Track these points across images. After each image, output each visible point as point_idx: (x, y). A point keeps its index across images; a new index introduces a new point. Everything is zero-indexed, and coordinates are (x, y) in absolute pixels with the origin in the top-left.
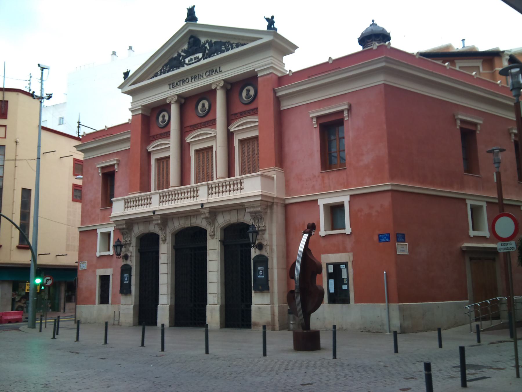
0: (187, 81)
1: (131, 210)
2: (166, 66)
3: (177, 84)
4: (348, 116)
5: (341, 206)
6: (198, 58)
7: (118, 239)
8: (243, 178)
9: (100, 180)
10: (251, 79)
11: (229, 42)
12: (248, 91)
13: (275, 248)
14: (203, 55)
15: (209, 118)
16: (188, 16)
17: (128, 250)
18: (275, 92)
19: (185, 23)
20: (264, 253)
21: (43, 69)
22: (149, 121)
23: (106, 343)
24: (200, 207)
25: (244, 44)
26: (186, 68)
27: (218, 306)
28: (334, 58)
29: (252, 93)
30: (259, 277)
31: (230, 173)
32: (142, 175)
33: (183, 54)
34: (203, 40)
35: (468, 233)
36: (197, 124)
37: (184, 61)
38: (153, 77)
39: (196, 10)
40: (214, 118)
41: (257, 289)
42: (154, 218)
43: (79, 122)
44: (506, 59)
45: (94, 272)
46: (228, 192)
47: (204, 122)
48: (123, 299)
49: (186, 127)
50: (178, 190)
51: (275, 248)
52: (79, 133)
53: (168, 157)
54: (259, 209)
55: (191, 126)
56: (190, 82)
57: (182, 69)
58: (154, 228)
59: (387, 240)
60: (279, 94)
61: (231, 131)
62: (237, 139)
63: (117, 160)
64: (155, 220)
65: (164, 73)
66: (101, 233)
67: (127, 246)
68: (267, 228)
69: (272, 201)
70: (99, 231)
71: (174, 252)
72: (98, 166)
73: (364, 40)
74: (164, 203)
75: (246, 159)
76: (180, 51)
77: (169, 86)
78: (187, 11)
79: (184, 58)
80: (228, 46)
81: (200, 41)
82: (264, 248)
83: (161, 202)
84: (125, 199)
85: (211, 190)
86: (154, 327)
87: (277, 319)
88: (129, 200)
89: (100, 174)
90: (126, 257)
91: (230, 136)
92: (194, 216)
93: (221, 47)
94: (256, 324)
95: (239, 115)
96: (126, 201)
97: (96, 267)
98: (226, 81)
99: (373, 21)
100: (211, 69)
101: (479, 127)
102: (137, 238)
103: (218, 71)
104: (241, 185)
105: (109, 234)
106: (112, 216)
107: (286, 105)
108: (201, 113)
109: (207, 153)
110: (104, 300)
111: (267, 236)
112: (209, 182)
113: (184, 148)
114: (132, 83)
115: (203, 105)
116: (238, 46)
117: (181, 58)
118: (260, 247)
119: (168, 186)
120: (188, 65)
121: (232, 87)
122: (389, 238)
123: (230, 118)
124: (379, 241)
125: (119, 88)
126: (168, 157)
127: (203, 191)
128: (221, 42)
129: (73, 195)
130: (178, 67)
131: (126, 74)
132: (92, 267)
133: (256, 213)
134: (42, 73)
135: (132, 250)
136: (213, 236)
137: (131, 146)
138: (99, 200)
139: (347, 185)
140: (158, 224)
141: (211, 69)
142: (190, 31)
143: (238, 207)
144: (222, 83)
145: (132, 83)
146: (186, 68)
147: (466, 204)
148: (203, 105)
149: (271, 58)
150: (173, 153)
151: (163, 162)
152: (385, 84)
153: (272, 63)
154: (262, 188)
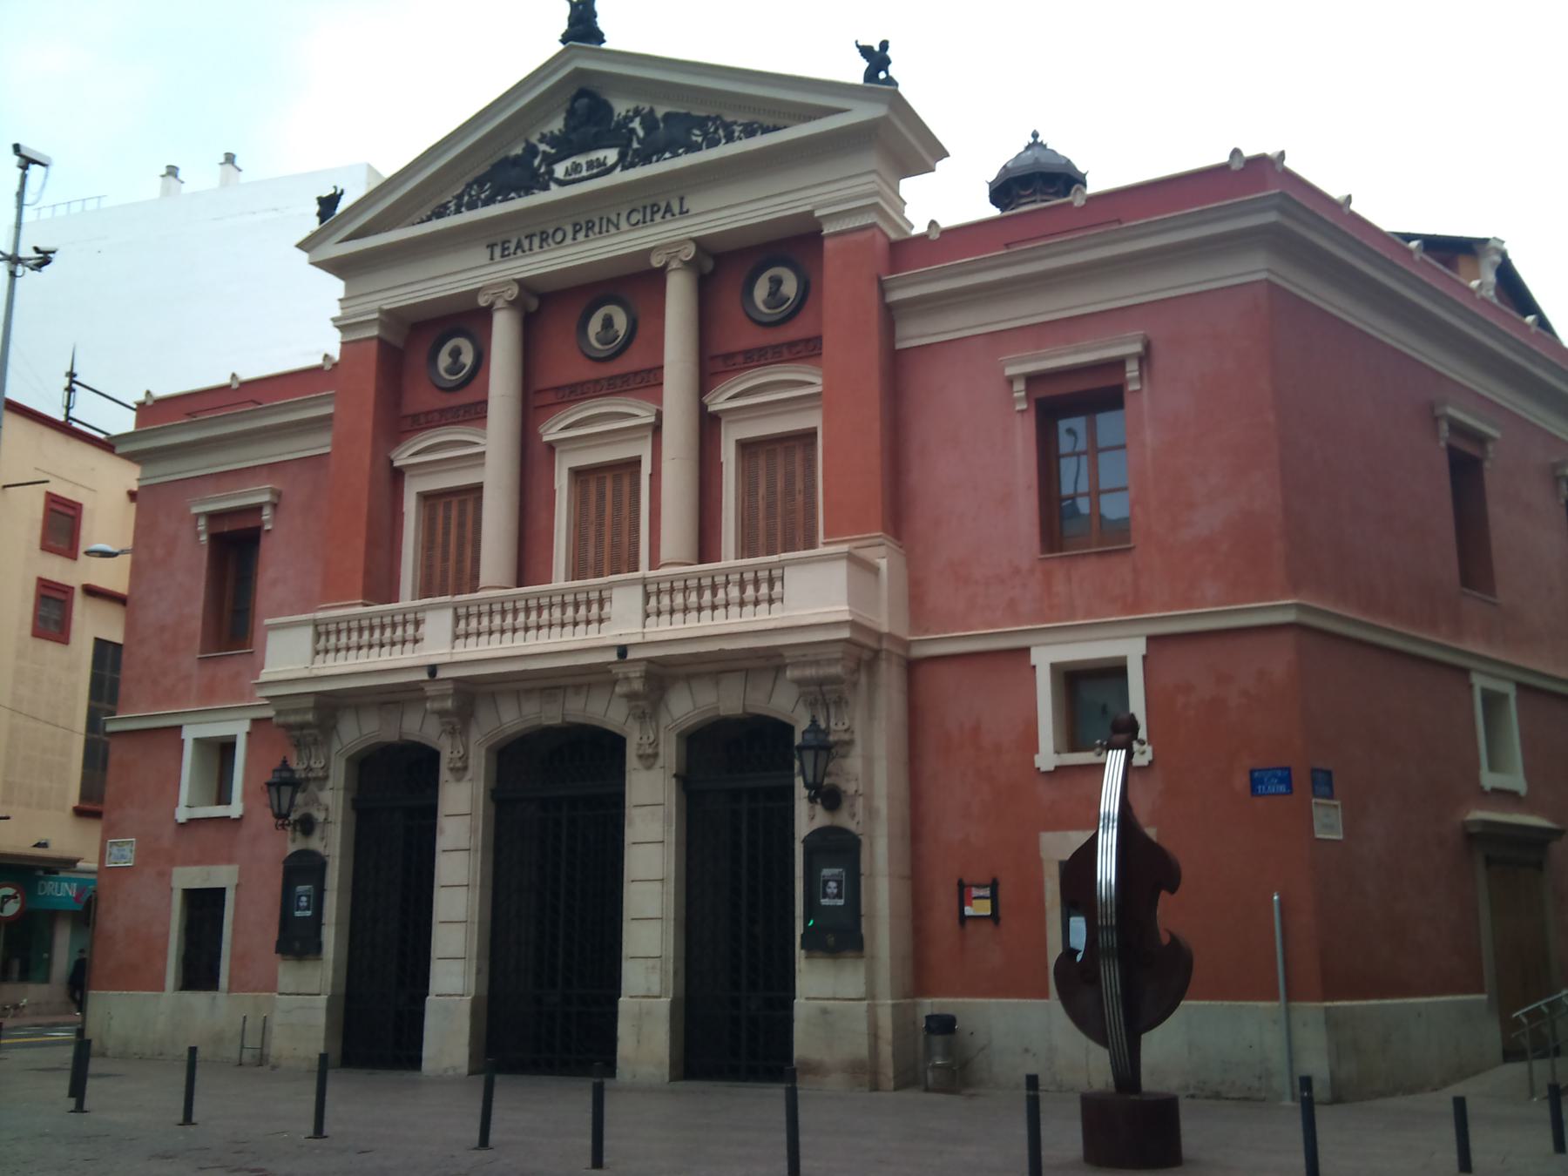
0: (559, 236)
1: (341, 662)
3: (519, 246)
4: (1141, 377)
5: (1115, 671)
7: (285, 762)
8: (782, 565)
9: (204, 555)
10: (798, 243)
11: (718, 117)
12: (777, 282)
13: (882, 804)
14: (622, 156)
15: (632, 362)
16: (570, 25)
17: (316, 801)
18: (883, 291)
19: (561, 47)
20: (843, 820)
21: (27, 162)
22: (407, 364)
23: (319, 1131)
24: (425, 677)
25: (776, 129)
26: (555, 193)
27: (665, 1001)
28: (945, 223)
29: (467, 358)
30: (825, 902)
31: (706, 548)
32: (371, 543)
33: (543, 147)
34: (621, 107)
35: (1477, 778)
36: (583, 384)
37: (550, 172)
38: (429, 219)
40: (479, 398)
41: (814, 944)
42: (430, 690)
43: (71, 375)
44: (1494, 263)
45: (165, 876)
46: (694, 614)
47: (611, 378)
48: (289, 974)
49: (540, 391)
50: (359, 617)
51: (882, 804)
52: (68, 408)
53: (477, 489)
54: (836, 670)
55: (557, 389)
56: (569, 241)
58: (418, 727)
59: (1282, 788)
60: (895, 296)
61: (711, 409)
63: (273, 492)
64: (433, 698)
65: (472, 206)
66: (197, 740)
67: (312, 787)
68: (858, 738)
69: (872, 643)
70: (189, 734)
71: (492, 812)
72: (195, 510)
73: (1002, 191)
75: (761, 504)
76: (534, 139)
77: (488, 252)
79: (551, 161)
80: (714, 128)
81: (610, 110)
82: (845, 805)
83: (317, 653)
84: (316, 624)
85: (653, 601)
86: (408, 1075)
87: (886, 1050)
88: (332, 627)
89: (204, 538)
90: (307, 826)
91: (708, 426)
92: (577, 688)
93: (689, 132)
94: (814, 1069)
95: (740, 359)
96: (322, 629)
97: (173, 861)
98: (526, 286)
99: (1035, 135)
101: (1490, 447)
102: (350, 760)
103: (676, 209)
104: (417, 629)
105: (226, 747)
106: (263, 678)
107: (913, 334)
108: (448, 377)
109: (617, 479)
110: (200, 971)
111: (854, 763)
112: (775, 558)
113: (532, 460)
114: (350, 235)
115: (608, 322)
116: (750, 132)
117: (536, 162)
118: (830, 798)
119: (393, 596)
120: (561, 183)
121: (722, 266)
122: (1287, 780)
123: (712, 366)
124: (1254, 790)
125: (301, 246)
126: (477, 489)
127: (437, 625)
128: (687, 115)
129: (38, 618)
130: (528, 191)
131: (328, 204)
132: (156, 859)
133: (820, 682)
134: (24, 178)
135: (331, 802)
136: (649, 759)
137: (336, 444)
138: (197, 625)
139: (1134, 602)
140: (442, 713)
141: (652, 202)
142: (579, 73)
143: (764, 662)
144: (515, 290)
145: (350, 235)
146: (555, 193)
147: (1471, 686)
148: (608, 322)
149: (873, 177)
150: (496, 479)
151: (447, 507)
152: (1267, 280)
153: (877, 193)
154: (853, 598)
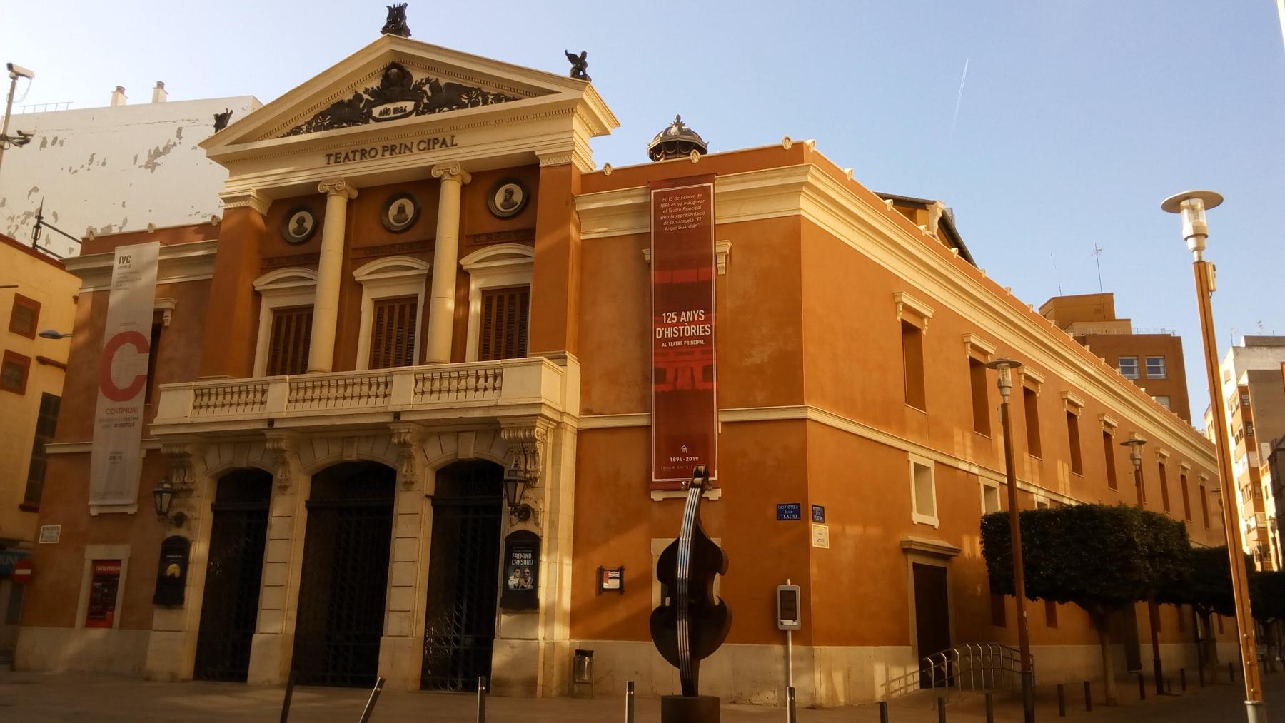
0: (373, 153)
2: (324, 117)
6: (402, 110)
14: (416, 107)
24: (266, 426)
25: (514, 99)
28: (614, 166)
29: (309, 225)
33: (366, 97)
34: (418, 77)
38: (289, 135)
39: (407, 12)
42: (269, 435)
56: (379, 156)
57: (361, 128)
59: (795, 516)
62: (474, 286)
65: (317, 129)
74: (249, 407)
78: (387, 13)
79: (371, 105)
100: (431, 137)
103: (449, 143)
110: (99, 613)
115: (402, 210)
116: (498, 99)
118: (526, 513)
120: (377, 120)
124: (779, 518)
131: (221, 120)
132: (74, 539)
146: (372, 126)
